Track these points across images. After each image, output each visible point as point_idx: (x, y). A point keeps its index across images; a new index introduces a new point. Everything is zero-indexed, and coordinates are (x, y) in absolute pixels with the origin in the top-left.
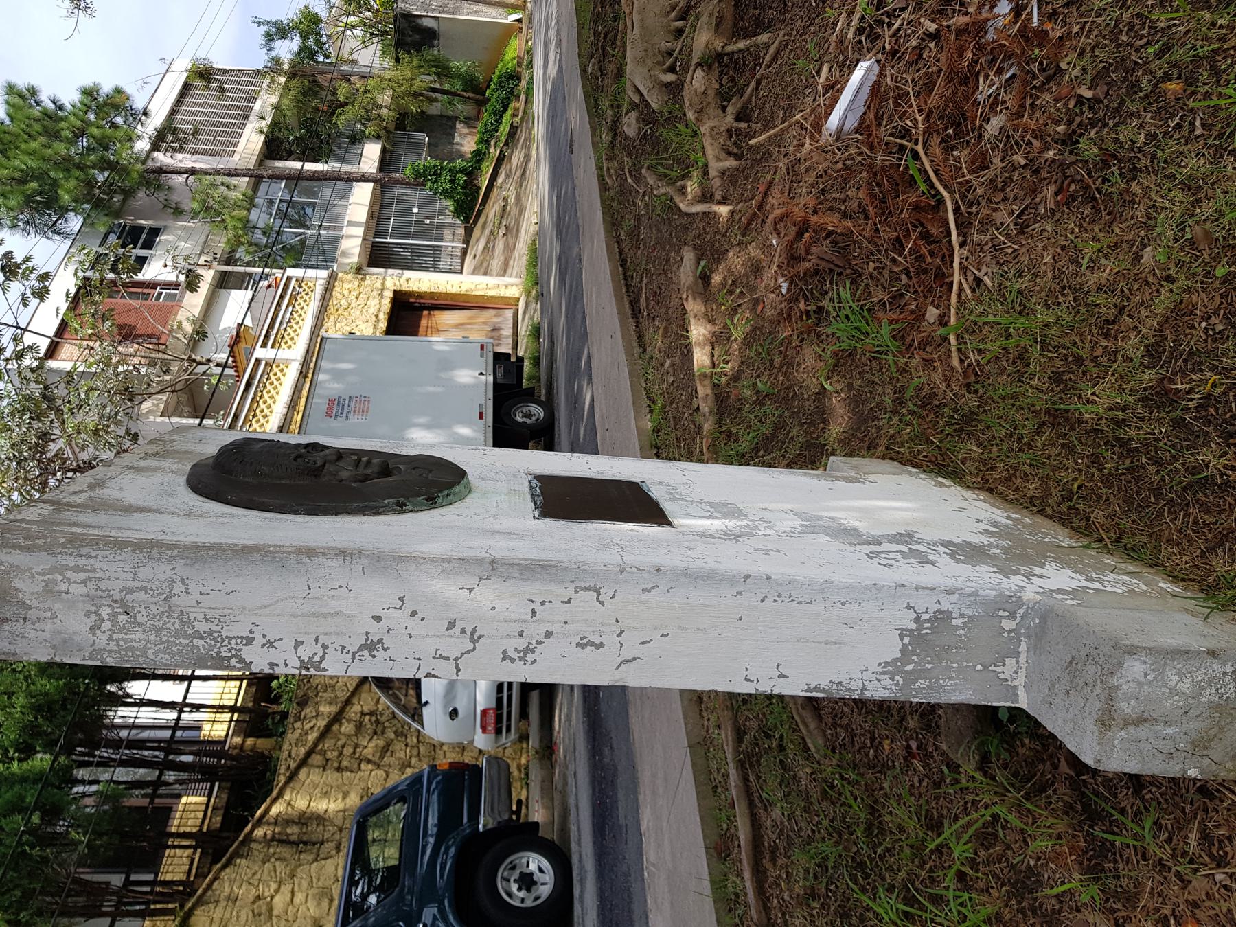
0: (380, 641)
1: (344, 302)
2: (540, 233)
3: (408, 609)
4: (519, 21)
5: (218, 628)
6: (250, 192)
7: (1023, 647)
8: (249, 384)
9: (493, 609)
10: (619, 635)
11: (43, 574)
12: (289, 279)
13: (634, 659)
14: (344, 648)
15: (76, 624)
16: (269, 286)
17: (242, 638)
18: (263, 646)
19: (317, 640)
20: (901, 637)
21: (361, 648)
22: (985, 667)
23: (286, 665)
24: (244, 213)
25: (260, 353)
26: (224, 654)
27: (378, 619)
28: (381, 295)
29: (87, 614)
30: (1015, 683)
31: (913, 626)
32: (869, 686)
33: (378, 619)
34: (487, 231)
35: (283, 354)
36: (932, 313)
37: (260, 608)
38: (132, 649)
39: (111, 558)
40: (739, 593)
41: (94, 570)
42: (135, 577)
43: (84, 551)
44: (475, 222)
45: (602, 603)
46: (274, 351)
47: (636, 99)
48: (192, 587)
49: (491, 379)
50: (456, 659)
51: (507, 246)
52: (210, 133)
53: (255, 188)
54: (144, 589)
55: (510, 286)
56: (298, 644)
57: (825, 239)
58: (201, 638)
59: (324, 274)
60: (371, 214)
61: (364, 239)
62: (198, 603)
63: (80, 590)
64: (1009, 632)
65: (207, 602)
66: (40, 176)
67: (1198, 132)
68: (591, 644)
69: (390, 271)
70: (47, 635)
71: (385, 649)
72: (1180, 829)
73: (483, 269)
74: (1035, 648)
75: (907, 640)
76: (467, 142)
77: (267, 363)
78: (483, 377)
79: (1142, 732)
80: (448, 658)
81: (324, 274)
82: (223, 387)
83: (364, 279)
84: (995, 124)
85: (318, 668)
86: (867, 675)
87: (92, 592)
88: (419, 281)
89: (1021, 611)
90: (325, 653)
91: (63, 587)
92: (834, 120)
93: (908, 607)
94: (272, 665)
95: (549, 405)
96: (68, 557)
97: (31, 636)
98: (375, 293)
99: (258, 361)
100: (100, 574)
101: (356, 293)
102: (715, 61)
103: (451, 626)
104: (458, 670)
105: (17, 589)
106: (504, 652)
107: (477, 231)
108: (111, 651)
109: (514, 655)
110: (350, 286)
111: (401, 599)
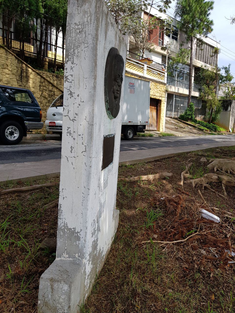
0: (72, 96)
1: (158, 87)
2: (176, 137)
3: (81, 103)
4: (230, 132)
5: (76, 55)
6: (187, 63)
7: (71, 259)
8: (138, 63)
9: (81, 125)
10: (74, 157)
11: (89, 11)
12: (164, 73)
13: (68, 161)
14: (71, 87)
15: (77, 19)
16: (162, 68)
17: (73, 61)
18: (71, 67)
19: (73, 80)
20: (74, 228)
21: (71, 92)
22: (66, 249)
23: (66, 72)
24: (181, 62)
25: (146, 66)
26: (69, 57)
27: (78, 96)
28: (160, 97)
29: (79, 22)
30: (62, 257)
31: (76, 231)
32: (61, 220)
33: (78, 96)
34: (176, 123)
35: (145, 72)
36: (156, 236)
37: (81, 66)
38: (70, 34)
39: (94, 28)
40: (85, 187)
41: (90, 24)
42: (89, 34)
43: (95, 21)
44: (179, 120)
45: (82, 152)
46: (146, 70)
47: (210, 161)
48: (86, 49)
49: (139, 124)
50: (68, 116)
51: (173, 128)
52: (201, 53)
53: (187, 65)
54: (86, 36)
55: (163, 129)
56: (72, 75)
57: (175, 209)
58: (73, 51)
59: (166, 82)
60: (181, 94)
61: (174, 92)
62: (82, 50)
63: (86, 20)
64: (75, 256)
65: (83, 52)
66: (190, 10)
67: (202, 303)
68: (72, 150)
69: (166, 99)
70: (74, 12)
71: (70, 97)
72: (25, 299)
73: (167, 122)
74: (71, 262)
75: (73, 230)
76: (199, 118)
77: (143, 68)
78: (139, 122)
79: (50, 289)
80: (68, 113)
81: (166, 82)
82: (137, 56)
83: (164, 92)
84: (204, 252)
85: (66, 81)
86: (64, 220)
87: (85, 23)
88: (164, 106)
89: (80, 259)
90: (69, 82)
91: (86, 16)
92: (205, 211)
93: (81, 230)
94: (66, 69)
95: (132, 139)
96: (94, 17)
97: (74, 8)
98: (161, 95)
99: (143, 65)
100: (89, 25)
101: (161, 90)
102: (220, 181)
103: (76, 114)
104: (65, 116)
105: (86, 4)
106: (70, 128)
107: (176, 121)
108: (70, 28)
109: (69, 130)
110: (163, 89)
111: (83, 102)
